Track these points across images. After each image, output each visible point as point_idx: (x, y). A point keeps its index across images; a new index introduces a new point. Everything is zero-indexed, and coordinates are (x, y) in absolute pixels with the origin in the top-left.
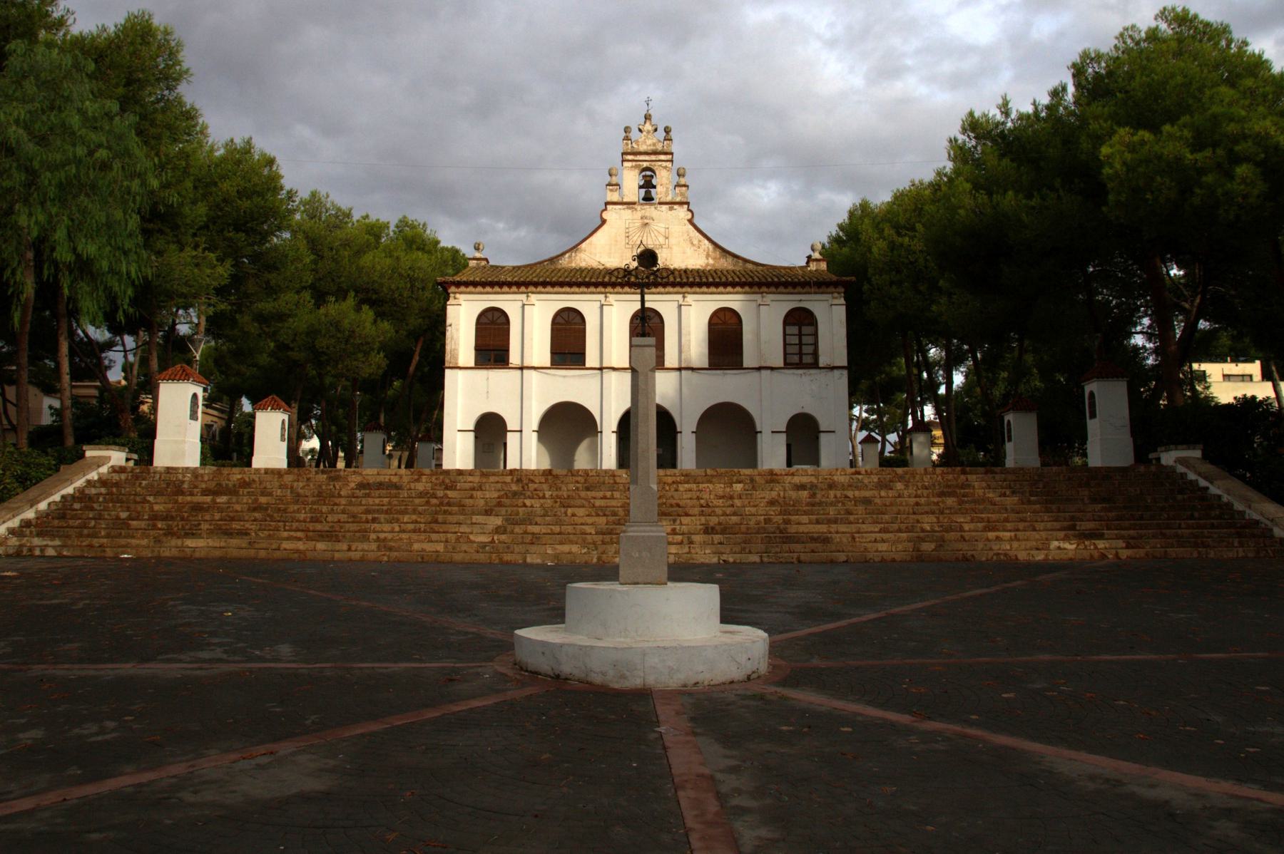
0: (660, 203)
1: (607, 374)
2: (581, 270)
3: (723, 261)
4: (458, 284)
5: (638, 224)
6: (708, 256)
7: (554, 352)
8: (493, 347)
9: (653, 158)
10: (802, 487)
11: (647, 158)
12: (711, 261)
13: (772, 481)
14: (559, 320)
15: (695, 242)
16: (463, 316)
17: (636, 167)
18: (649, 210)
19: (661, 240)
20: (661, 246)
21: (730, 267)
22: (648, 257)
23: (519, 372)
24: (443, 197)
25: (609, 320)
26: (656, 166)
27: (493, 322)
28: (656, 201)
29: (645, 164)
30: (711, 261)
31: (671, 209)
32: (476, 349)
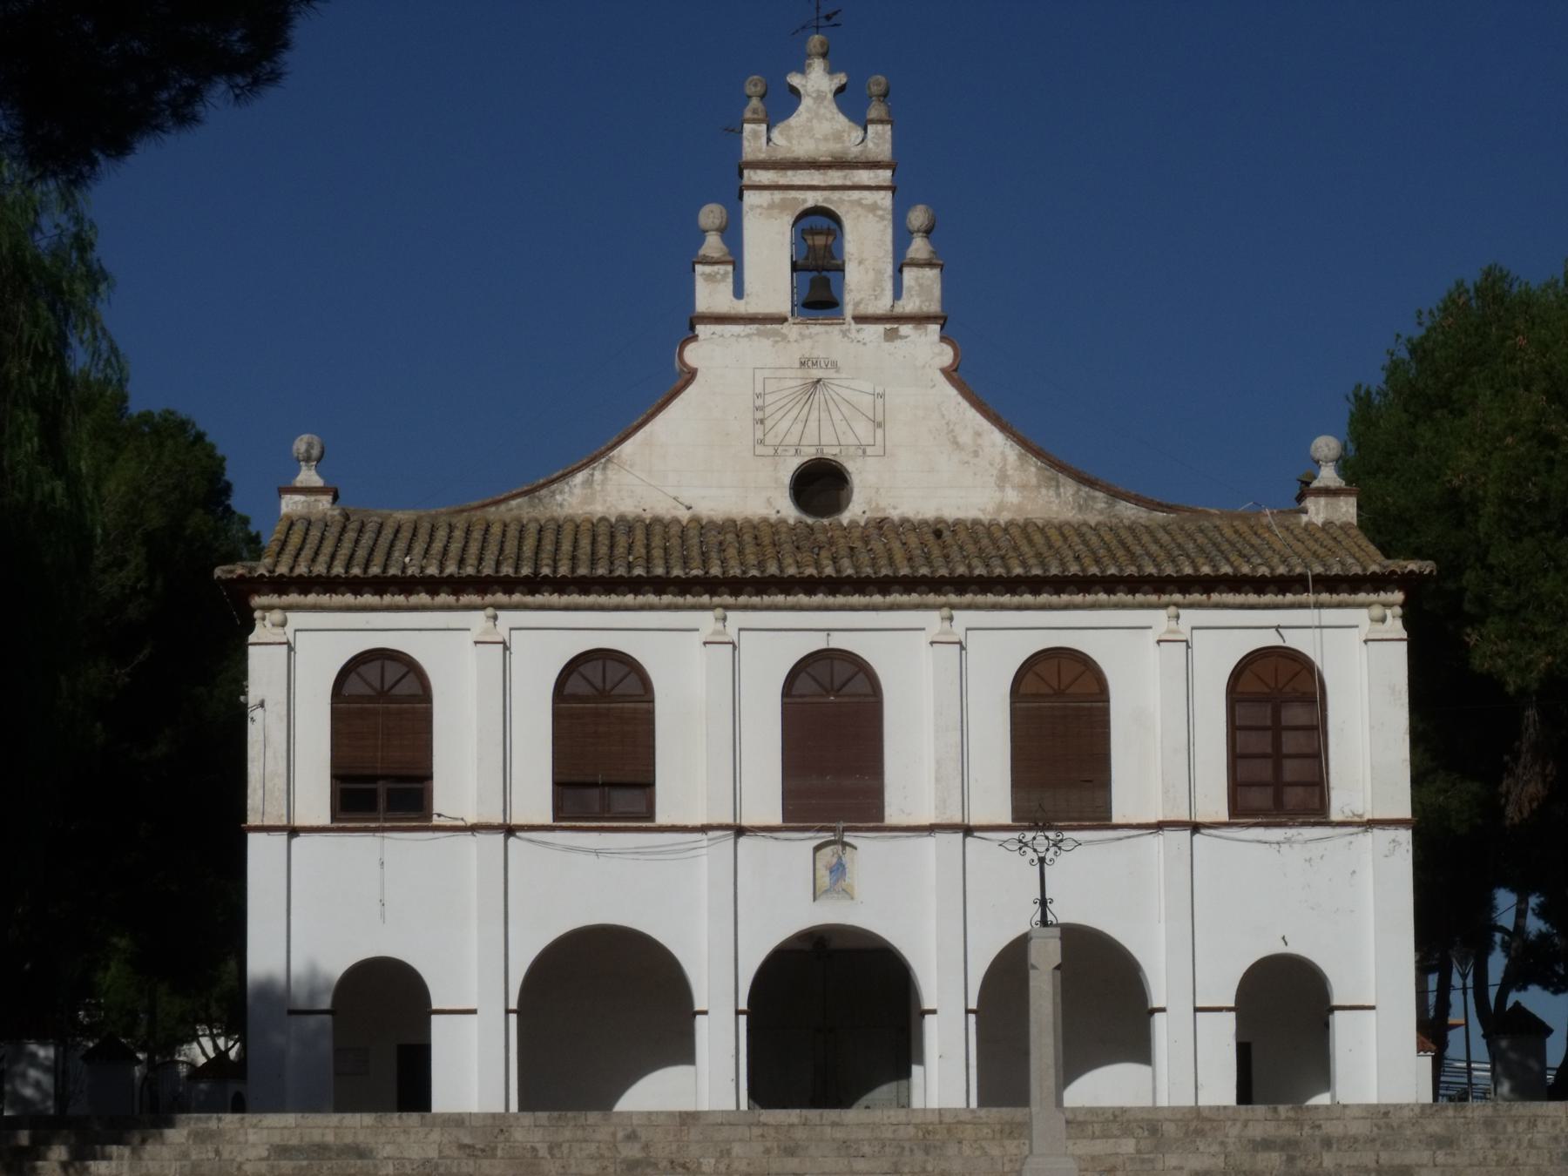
0: (861, 319)
1: (299, 842)
2: (652, 528)
3: (1047, 494)
4: (280, 585)
5: (794, 380)
6: (1003, 479)
7: (1237, 786)
8: (384, 775)
9: (835, 177)
10: (1267, 1145)
11: (815, 178)
12: (1012, 496)
13: (1200, 1133)
14: (1029, 686)
15: (965, 438)
16: (293, 669)
17: (783, 206)
18: (822, 338)
19: (863, 430)
20: (863, 449)
21: (1070, 515)
22: (820, 483)
23: (282, 838)
24: (759, 334)
25: (715, 684)
26: (839, 203)
27: (383, 695)
28: (849, 311)
29: (812, 199)
30: (1012, 496)
31: (891, 336)
32: (335, 777)
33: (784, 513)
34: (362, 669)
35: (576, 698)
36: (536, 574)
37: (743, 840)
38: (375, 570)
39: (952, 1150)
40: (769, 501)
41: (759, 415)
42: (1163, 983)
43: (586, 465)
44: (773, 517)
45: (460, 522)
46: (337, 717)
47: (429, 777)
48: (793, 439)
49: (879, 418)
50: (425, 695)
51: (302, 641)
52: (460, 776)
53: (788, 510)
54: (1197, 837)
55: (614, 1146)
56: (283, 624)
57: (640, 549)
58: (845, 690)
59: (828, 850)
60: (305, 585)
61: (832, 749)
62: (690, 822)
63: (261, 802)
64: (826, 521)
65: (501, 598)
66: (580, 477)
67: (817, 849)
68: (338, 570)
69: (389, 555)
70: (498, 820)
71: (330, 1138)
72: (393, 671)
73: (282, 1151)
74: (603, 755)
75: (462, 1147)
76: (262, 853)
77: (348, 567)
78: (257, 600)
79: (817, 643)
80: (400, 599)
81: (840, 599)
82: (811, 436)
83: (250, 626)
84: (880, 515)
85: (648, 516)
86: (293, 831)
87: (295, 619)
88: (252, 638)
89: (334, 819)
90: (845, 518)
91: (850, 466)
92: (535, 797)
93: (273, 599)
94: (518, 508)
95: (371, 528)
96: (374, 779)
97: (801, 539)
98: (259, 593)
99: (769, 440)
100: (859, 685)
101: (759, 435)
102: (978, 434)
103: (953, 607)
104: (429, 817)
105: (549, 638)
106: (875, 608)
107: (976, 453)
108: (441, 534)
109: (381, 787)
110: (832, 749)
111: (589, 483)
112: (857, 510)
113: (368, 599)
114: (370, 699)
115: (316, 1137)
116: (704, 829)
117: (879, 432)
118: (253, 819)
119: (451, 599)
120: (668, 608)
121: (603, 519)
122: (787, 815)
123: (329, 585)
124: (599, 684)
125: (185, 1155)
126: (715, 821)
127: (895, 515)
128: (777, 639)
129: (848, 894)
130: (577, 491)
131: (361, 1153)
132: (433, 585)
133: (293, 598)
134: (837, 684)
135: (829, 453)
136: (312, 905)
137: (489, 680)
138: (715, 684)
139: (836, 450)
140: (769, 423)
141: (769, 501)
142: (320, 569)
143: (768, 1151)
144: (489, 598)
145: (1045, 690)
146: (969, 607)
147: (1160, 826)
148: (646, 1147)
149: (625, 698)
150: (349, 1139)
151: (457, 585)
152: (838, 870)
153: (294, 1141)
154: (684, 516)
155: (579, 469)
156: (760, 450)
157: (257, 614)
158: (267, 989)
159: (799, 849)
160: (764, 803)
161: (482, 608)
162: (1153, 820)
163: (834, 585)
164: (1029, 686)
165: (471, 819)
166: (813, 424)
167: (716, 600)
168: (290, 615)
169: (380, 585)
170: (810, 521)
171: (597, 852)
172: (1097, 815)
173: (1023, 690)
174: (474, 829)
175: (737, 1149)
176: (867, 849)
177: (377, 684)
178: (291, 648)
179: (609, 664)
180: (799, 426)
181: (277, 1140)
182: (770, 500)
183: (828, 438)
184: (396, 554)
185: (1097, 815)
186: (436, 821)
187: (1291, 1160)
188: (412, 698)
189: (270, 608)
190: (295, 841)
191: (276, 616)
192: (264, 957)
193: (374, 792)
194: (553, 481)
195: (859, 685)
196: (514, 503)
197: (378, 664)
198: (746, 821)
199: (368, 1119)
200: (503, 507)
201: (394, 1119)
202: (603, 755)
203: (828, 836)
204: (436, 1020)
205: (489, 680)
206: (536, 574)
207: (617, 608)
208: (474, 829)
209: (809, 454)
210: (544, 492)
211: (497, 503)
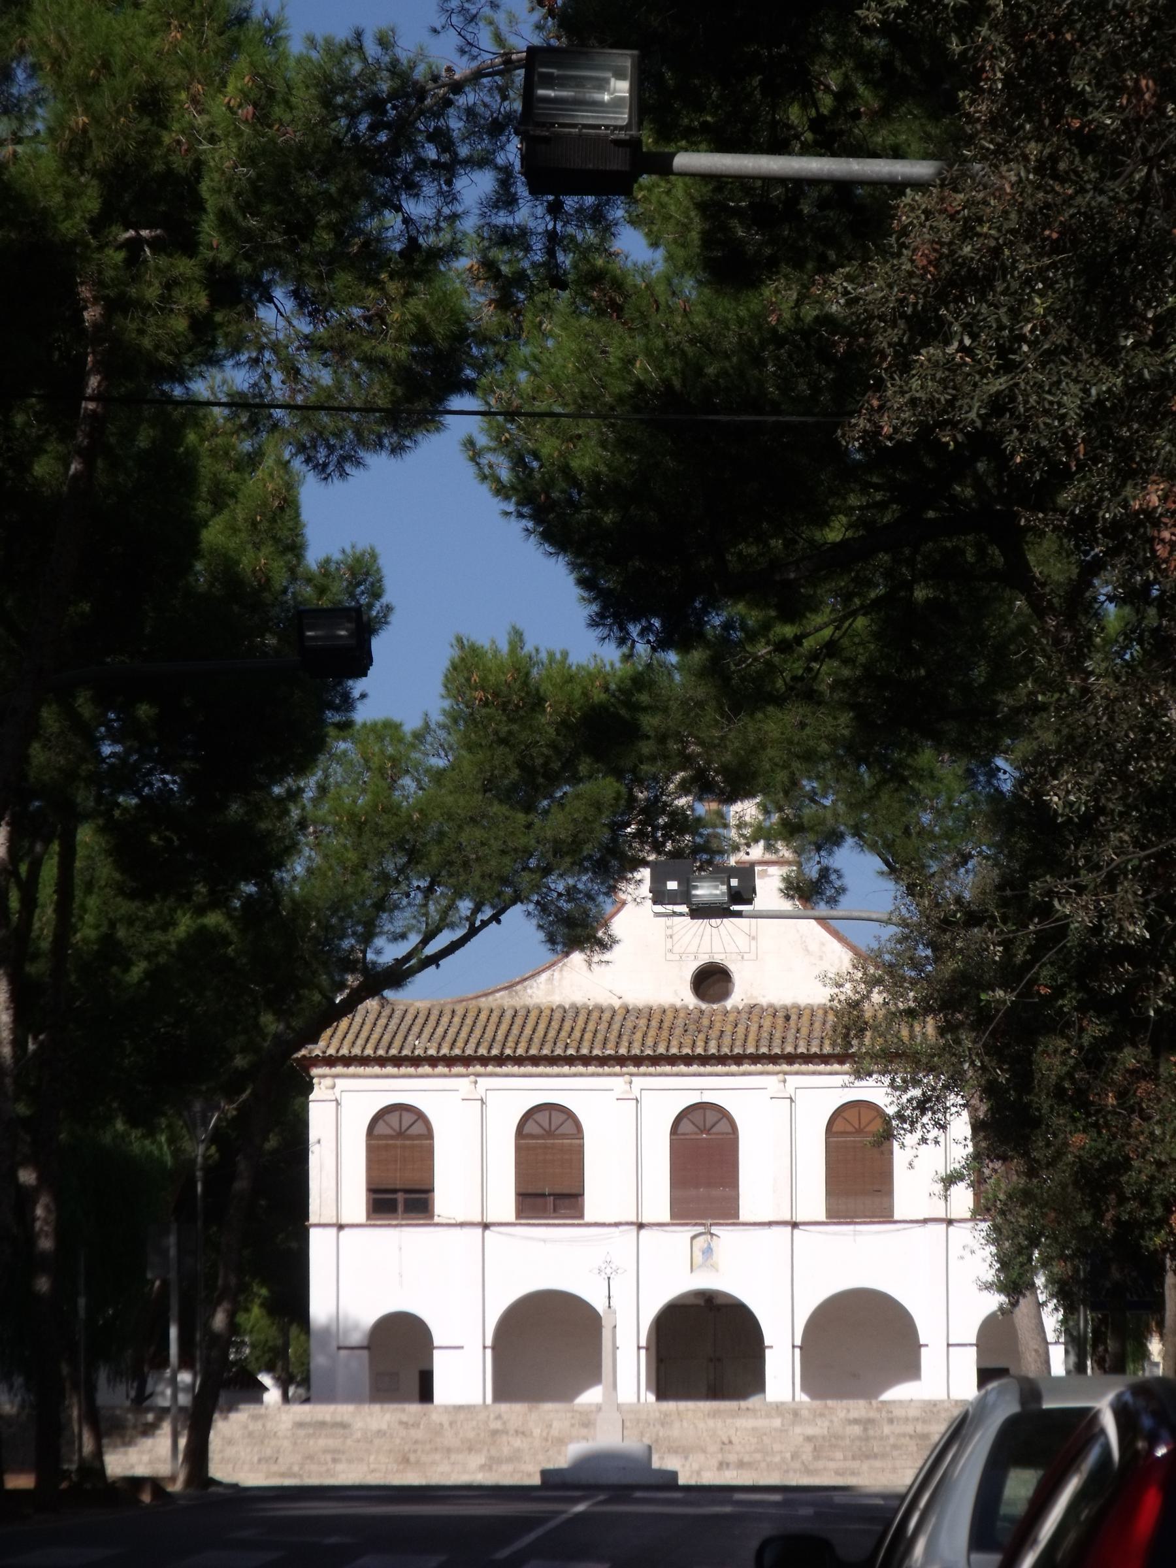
4: (330, 1061)
8: (401, 1190)
10: (856, 1421)
14: (839, 1126)
25: (625, 1125)
27: (401, 1134)
33: (686, 1002)
34: (386, 1117)
35: (531, 1136)
36: (502, 1053)
37: (643, 1232)
38: (393, 1052)
39: (677, 1425)
40: (676, 992)
41: (669, 932)
42: (928, 1330)
43: (548, 968)
44: (679, 1004)
45: (460, 1011)
46: (370, 1149)
47: (430, 1190)
48: (692, 949)
49: (753, 933)
50: (429, 1135)
51: (346, 1099)
52: (451, 1191)
53: (691, 1000)
54: (951, 1228)
55: (486, 1423)
56: (333, 1087)
57: (577, 1034)
58: (714, 1130)
59: (701, 1239)
60: (348, 1061)
61: (704, 1165)
62: (607, 1221)
63: (319, 1206)
64: (715, 1006)
65: (479, 1069)
66: (544, 976)
67: (693, 1238)
68: (369, 1051)
69: (406, 1038)
70: (478, 1219)
71: (328, 1418)
72: (408, 1118)
73: (300, 1425)
74: (550, 1179)
75: (401, 1423)
76: (320, 1243)
77: (376, 1049)
78: (315, 1071)
79: (694, 1098)
80: (411, 1070)
81: (709, 1069)
82: (705, 947)
83: (310, 1088)
84: (753, 1002)
85: (591, 1004)
86: (341, 1227)
87: (340, 1083)
88: (311, 1097)
89: (368, 1218)
90: (729, 1004)
91: (733, 967)
92: (504, 1203)
93: (325, 1070)
94: (502, 999)
95: (398, 1014)
96: (395, 1191)
97: (693, 1022)
98: (315, 1065)
99: (676, 949)
100: (723, 1126)
101: (669, 946)
102: (823, 944)
103: (785, 1073)
104: (432, 1217)
105: (514, 1094)
106: (733, 1075)
107: (821, 958)
108: (445, 1020)
109: (400, 1197)
110: (704, 1165)
111: (550, 980)
112: (737, 999)
113: (390, 1070)
114: (391, 1137)
115: (320, 1417)
116: (617, 1225)
117: (753, 943)
118: (313, 1219)
119: (446, 1070)
120: (592, 1075)
121: (559, 1006)
122: (673, 1215)
123: (364, 1061)
124: (546, 1126)
125: (246, 1427)
126: (623, 1220)
127: (764, 1001)
128: (668, 1094)
129: (714, 1267)
130: (542, 986)
131: (344, 1426)
132: (433, 1061)
133: (339, 1069)
134: (708, 1125)
135: (718, 959)
136: (353, 1274)
137: (473, 1123)
138: (625, 1125)
139: (722, 956)
140: (675, 938)
141: (676, 992)
142: (356, 1051)
143: (573, 1425)
144: (471, 1069)
145: (850, 1129)
146: (797, 1073)
147: (925, 1221)
148: (504, 1423)
149: (564, 1136)
150: (339, 1419)
151: (450, 1061)
152: (708, 1251)
153: (308, 1419)
154: (617, 1004)
155: (543, 971)
156: (670, 956)
157: (315, 1081)
158: (326, 1331)
159: (683, 1235)
160: (658, 1206)
161: (467, 1076)
162: (921, 1217)
163: (704, 1060)
164: (839, 1126)
165: (460, 1220)
166: (707, 938)
167: (625, 1069)
168: (338, 1081)
169: (398, 1061)
170: (704, 1006)
171: (544, 1241)
172: (885, 1215)
173: (835, 1129)
174: (462, 1225)
175: (556, 1424)
176: (727, 1237)
177: (397, 1127)
178: (338, 1103)
179: (554, 1113)
180: (697, 940)
181: (298, 1419)
182: (678, 993)
183: (717, 948)
184: (410, 1038)
185: (885, 1215)
186: (436, 1220)
187: (865, 1430)
188: (419, 1137)
189: (324, 1076)
190: (342, 1233)
191: (328, 1082)
192: (320, 1308)
193: (395, 1200)
194: (525, 980)
195: (723, 1126)
196: (498, 995)
197: (397, 1114)
198: (645, 1220)
199: (350, 1408)
200: (491, 998)
201: (366, 1408)
202: (550, 1179)
203: (701, 1229)
204: (436, 1352)
205: (473, 1123)
206: (502, 1053)
207: (558, 1076)
208: (462, 1225)
209: (704, 959)
210: (519, 987)
211: (486, 995)
